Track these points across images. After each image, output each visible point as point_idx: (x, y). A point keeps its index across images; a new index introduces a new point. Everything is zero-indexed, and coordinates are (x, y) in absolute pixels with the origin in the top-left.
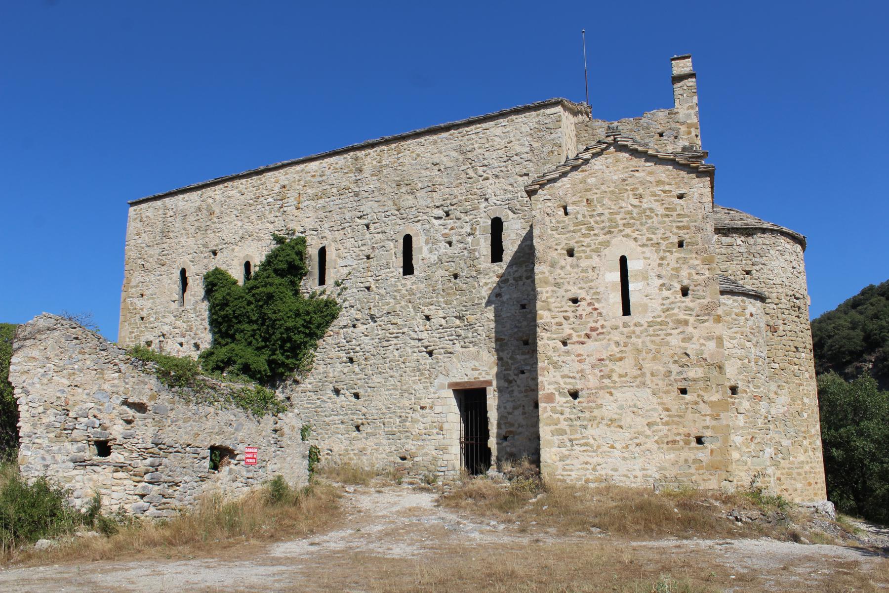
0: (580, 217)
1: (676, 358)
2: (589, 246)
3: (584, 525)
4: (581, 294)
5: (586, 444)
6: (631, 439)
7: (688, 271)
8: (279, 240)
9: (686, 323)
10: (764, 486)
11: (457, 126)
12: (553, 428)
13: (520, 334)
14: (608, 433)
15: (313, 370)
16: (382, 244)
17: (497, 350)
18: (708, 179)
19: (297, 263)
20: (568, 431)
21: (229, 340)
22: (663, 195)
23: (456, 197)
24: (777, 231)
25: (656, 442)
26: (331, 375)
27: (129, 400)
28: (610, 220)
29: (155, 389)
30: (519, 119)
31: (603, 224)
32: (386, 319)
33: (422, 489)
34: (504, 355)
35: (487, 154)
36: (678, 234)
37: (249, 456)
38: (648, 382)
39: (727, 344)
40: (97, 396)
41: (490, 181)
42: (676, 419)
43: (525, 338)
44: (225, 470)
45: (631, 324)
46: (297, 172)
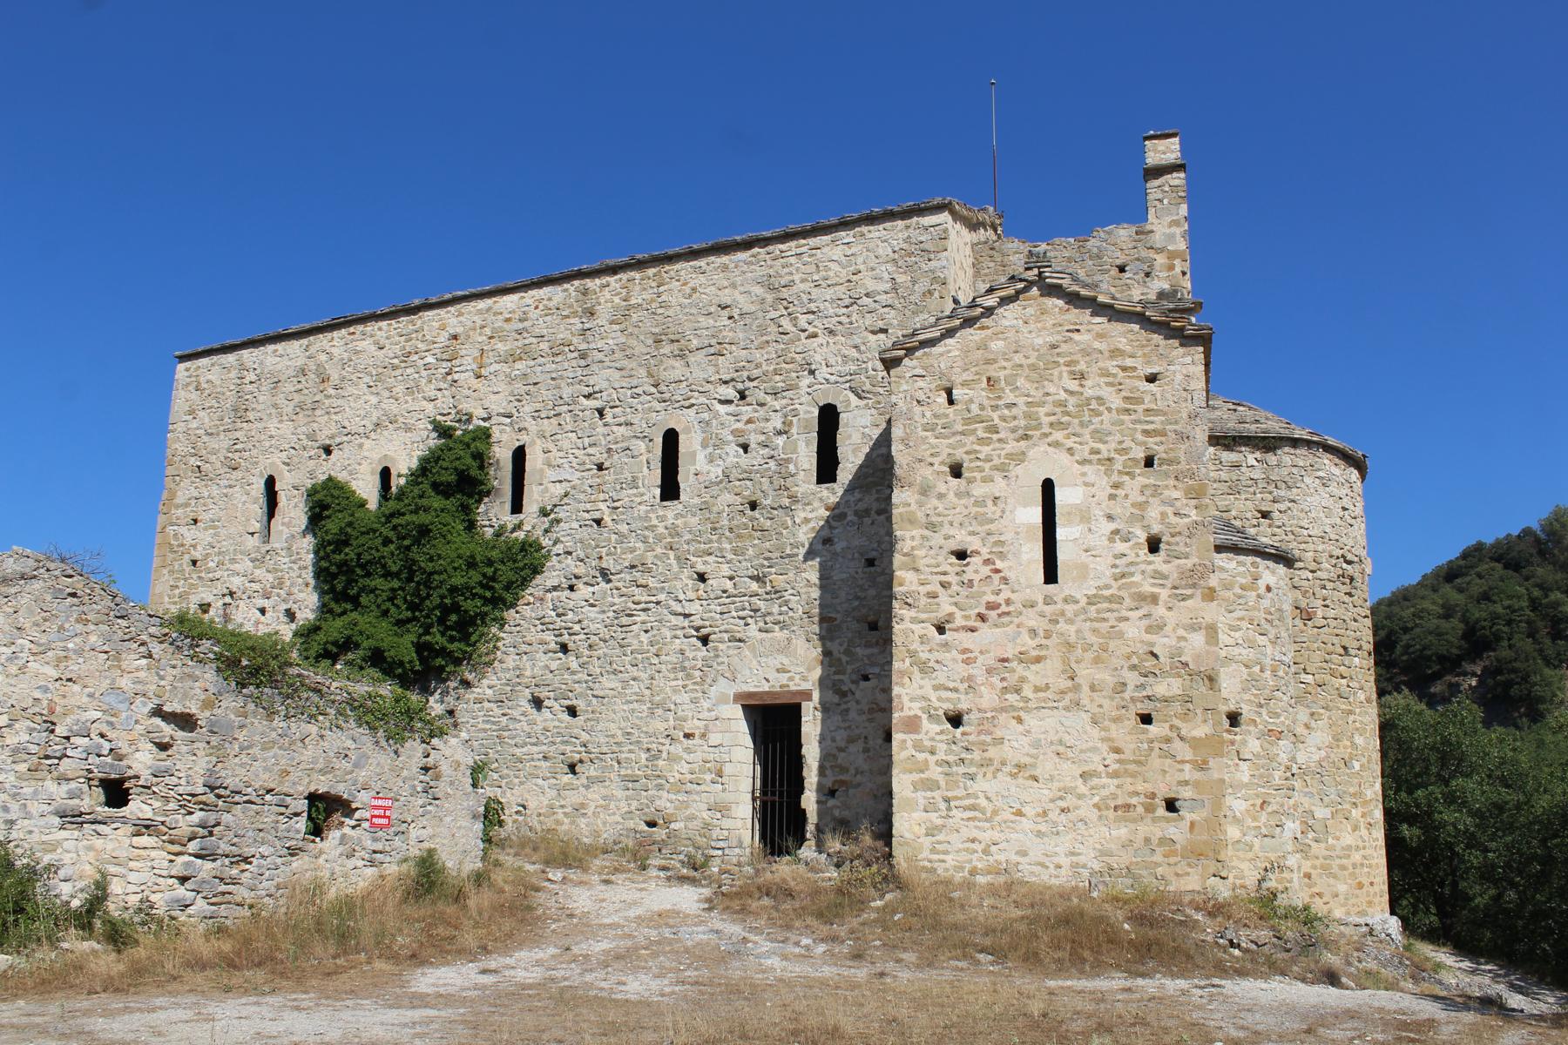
0: (975, 408)
1: (1135, 660)
2: (988, 459)
3: (965, 950)
4: (972, 544)
5: (973, 808)
6: (1052, 801)
7: (1162, 508)
8: (444, 432)
9: (1154, 599)
10: (1280, 888)
11: (764, 242)
12: (916, 777)
13: (864, 611)
14: (1013, 789)
15: (496, 664)
16: (624, 445)
17: (822, 638)
18: (1201, 349)
19: (474, 472)
20: (943, 784)
21: (349, 606)
22: (1121, 374)
23: (758, 366)
24: (1317, 444)
25: (1096, 806)
26: (528, 673)
27: (165, 708)
28: (1028, 416)
29: (212, 690)
30: (875, 232)
31: (1015, 423)
32: (628, 578)
33: (683, 879)
34: (834, 647)
36: (1145, 443)
37: (376, 812)
38: (1085, 701)
39: (1223, 638)
40: (107, 699)
41: (819, 340)
42: (1133, 767)
44: (334, 835)
46: (480, 312)
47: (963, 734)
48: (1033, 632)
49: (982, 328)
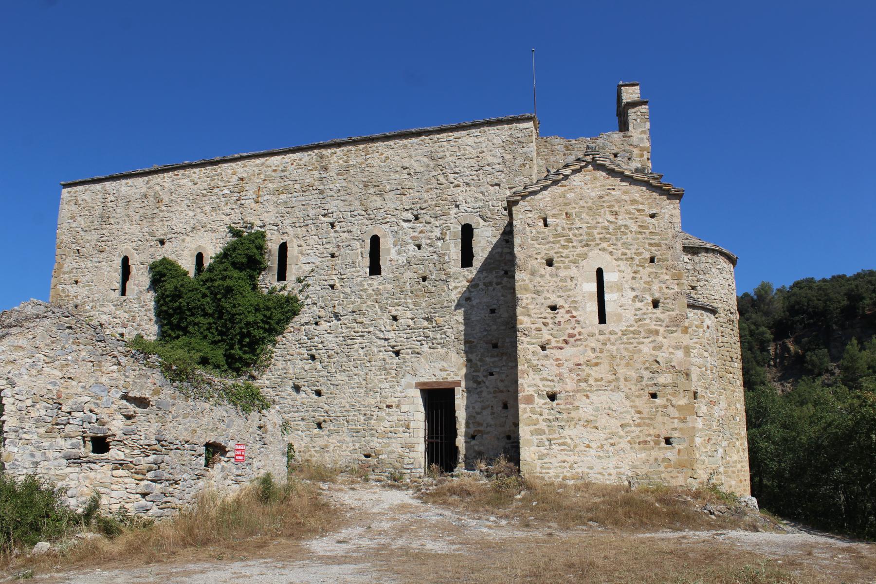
0: (559, 229)
1: (647, 365)
3: (580, 519)
4: (560, 302)
5: (564, 444)
6: (606, 440)
7: (660, 285)
8: (236, 233)
9: (657, 332)
12: (532, 428)
13: (490, 337)
14: (585, 434)
15: (271, 366)
16: (347, 243)
17: (466, 352)
19: (258, 257)
20: (547, 431)
21: (181, 333)
22: (637, 213)
23: (426, 202)
24: (717, 251)
25: (629, 442)
26: (291, 371)
27: (130, 395)
28: (588, 234)
29: (159, 383)
30: (492, 130)
32: (351, 318)
33: (391, 487)
34: (473, 357)
35: (458, 162)
37: (238, 453)
38: (622, 387)
40: (93, 389)
41: (461, 188)
42: (647, 421)
43: (494, 341)
44: (218, 466)
45: (606, 332)
46: (257, 165)
47: (557, 404)
48: (594, 350)
49: (562, 186)
